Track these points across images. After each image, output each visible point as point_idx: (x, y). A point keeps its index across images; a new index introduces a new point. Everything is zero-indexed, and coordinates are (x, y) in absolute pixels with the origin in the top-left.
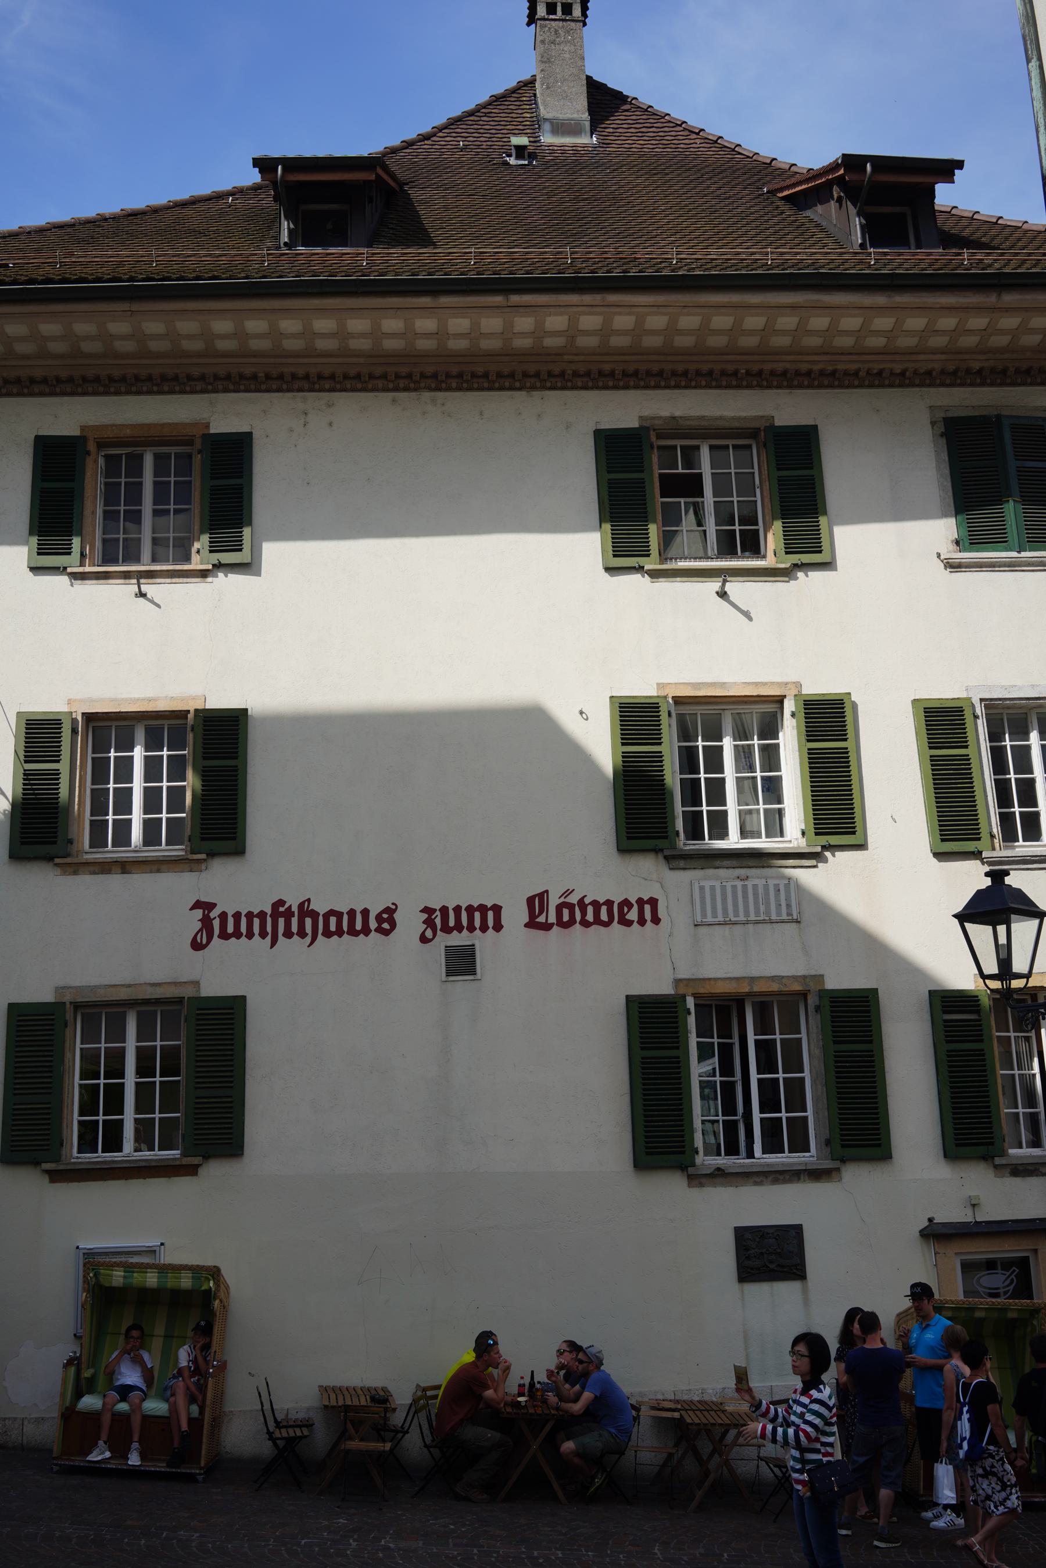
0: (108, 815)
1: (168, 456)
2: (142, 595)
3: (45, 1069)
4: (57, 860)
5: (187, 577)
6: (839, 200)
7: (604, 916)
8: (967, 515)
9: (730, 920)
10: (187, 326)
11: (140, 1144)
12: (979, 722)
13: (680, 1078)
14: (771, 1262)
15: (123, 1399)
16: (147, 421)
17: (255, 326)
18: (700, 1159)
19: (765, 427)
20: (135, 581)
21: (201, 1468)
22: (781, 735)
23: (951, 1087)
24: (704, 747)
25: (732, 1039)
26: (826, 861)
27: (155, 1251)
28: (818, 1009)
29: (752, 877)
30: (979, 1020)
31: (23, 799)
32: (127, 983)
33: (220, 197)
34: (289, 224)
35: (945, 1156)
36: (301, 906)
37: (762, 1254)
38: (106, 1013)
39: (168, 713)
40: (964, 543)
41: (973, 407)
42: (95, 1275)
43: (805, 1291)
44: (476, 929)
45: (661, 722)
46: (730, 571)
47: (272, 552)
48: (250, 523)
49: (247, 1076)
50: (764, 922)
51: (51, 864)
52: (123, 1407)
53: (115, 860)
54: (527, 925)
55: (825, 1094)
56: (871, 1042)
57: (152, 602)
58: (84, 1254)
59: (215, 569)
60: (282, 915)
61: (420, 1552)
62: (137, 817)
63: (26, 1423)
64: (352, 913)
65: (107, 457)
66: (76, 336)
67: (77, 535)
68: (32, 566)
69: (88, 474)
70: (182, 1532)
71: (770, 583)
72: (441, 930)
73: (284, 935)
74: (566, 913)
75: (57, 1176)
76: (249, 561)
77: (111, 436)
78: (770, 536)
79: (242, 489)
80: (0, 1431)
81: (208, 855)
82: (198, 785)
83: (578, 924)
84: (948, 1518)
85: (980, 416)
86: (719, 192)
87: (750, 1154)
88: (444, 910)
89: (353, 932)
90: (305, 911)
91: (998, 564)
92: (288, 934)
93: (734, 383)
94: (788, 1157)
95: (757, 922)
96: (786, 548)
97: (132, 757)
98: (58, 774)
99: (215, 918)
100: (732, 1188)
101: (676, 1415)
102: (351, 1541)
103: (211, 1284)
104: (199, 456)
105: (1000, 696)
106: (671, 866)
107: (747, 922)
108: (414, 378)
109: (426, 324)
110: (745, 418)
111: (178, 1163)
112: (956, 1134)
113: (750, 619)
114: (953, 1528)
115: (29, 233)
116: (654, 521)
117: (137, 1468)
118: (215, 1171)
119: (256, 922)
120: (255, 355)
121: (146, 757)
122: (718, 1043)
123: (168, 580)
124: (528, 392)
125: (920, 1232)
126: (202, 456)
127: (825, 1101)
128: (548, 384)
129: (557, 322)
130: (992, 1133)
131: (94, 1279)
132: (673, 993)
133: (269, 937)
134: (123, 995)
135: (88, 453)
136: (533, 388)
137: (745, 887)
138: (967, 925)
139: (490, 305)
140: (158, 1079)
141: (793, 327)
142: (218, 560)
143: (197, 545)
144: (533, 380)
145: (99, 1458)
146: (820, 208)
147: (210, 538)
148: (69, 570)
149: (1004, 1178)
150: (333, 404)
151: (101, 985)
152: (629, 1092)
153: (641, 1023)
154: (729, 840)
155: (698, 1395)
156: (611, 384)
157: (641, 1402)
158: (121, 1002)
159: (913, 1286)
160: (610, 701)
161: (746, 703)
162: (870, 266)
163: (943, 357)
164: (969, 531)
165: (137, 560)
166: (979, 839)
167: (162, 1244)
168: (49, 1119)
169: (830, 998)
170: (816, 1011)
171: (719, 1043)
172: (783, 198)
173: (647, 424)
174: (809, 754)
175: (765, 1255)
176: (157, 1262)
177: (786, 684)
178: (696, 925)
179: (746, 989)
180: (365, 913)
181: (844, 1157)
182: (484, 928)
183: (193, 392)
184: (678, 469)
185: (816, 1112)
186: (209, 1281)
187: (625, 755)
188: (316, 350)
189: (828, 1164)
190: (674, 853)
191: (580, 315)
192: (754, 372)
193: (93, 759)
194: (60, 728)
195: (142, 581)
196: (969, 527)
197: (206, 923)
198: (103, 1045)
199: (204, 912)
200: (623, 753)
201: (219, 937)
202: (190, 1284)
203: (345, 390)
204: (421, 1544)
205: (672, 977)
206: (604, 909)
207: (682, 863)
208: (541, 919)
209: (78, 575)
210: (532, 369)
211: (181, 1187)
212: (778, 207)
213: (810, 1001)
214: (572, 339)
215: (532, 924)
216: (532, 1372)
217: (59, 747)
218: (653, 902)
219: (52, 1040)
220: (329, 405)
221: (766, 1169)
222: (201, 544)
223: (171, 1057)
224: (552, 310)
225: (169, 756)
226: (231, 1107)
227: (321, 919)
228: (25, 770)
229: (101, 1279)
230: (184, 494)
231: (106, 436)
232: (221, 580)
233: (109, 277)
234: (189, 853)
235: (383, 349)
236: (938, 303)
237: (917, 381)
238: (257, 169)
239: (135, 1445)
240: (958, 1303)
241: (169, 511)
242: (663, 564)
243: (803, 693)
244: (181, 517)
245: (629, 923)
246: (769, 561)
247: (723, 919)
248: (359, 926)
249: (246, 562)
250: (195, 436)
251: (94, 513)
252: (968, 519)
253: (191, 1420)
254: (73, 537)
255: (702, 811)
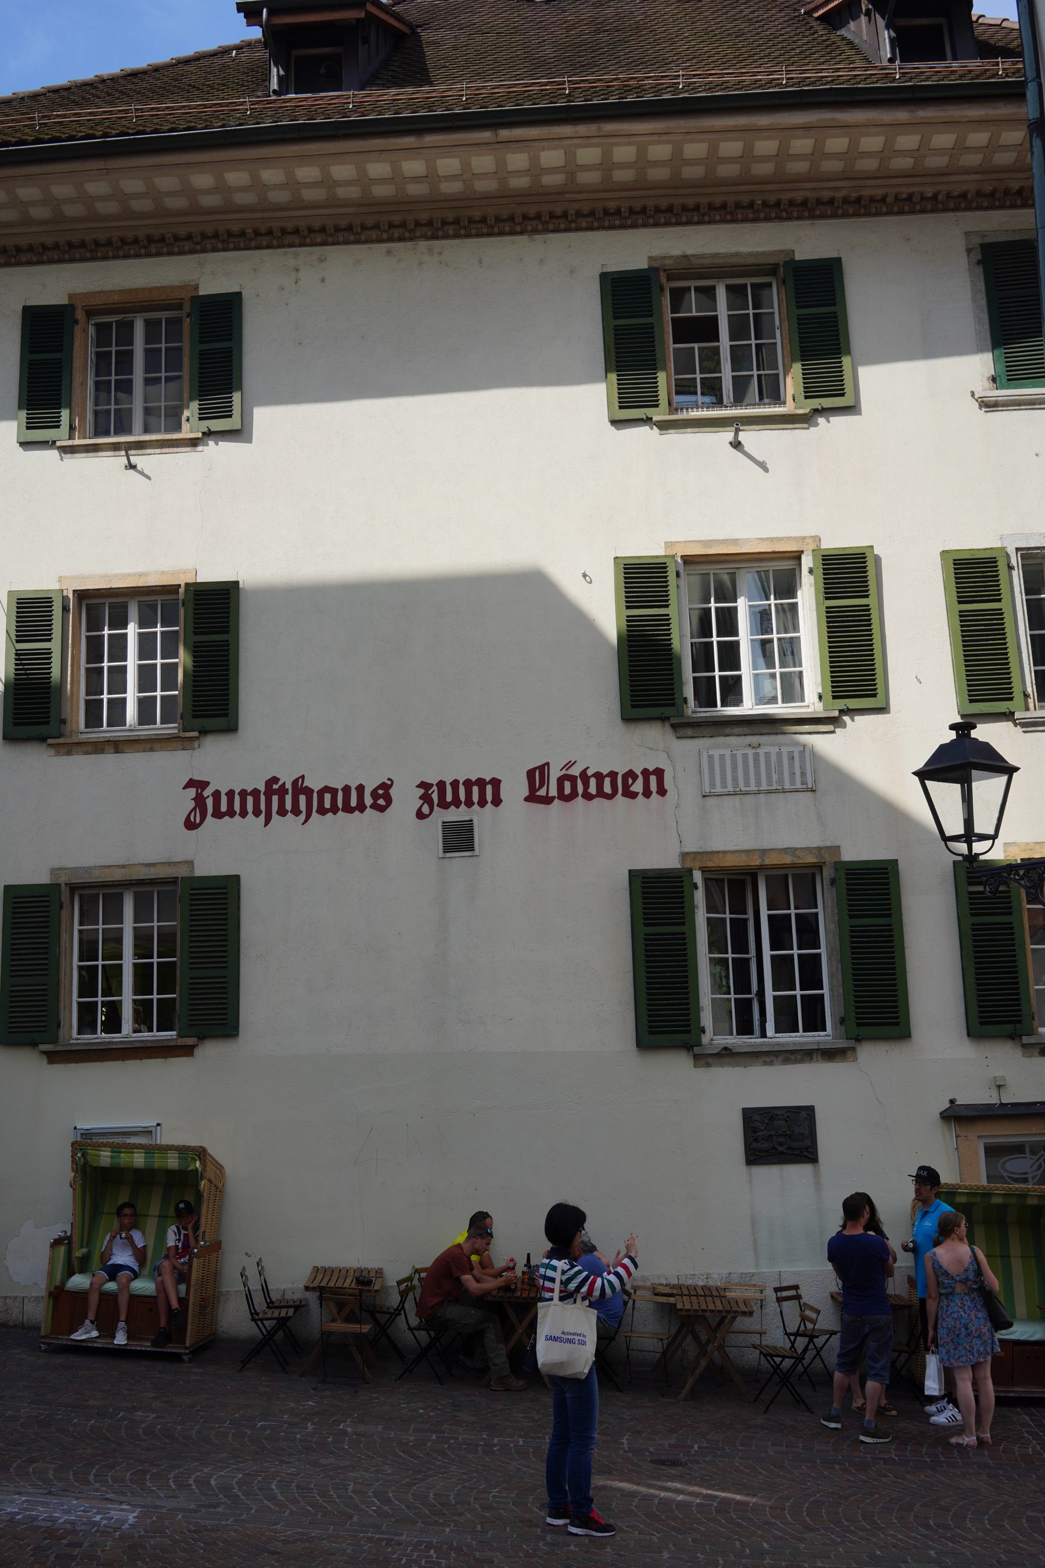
0: (102, 694)
1: (159, 321)
2: (132, 467)
3: (41, 951)
4: (50, 741)
5: (177, 446)
6: (868, 13)
7: (607, 789)
8: (1005, 349)
9: (741, 791)
10: (166, 182)
11: (140, 1025)
12: (1015, 573)
13: (685, 955)
14: (781, 1144)
15: (112, 1278)
16: (135, 286)
17: (236, 178)
18: (705, 1039)
19: (785, 262)
20: (123, 453)
21: (186, 1348)
22: (799, 593)
23: (976, 963)
24: (717, 609)
25: (746, 914)
26: (844, 725)
27: (151, 1131)
28: (833, 882)
29: (765, 745)
30: (1009, 892)
31: (16, 679)
32: (121, 863)
33: (225, 52)
34: (278, 71)
35: (969, 1035)
36: (295, 783)
37: (771, 1136)
38: (103, 894)
39: (159, 588)
40: (1001, 379)
41: (1014, 231)
42: (83, 1155)
43: (817, 1175)
44: (474, 804)
45: (669, 583)
46: (745, 420)
47: (263, 417)
48: (240, 388)
49: (242, 956)
50: (776, 791)
51: (45, 745)
52: (111, 1286)
53: (107, 739)
54: (527, 799)
55: (840, 971)
56: (889, 916)
57: (142, 473)
58: (82, 1134)
59: (206, 438)
60: (276, 792)
61: (375, 1437)
62: (131, 695)
63: (26, 1301)
64: (347, 789)
65: (98, 326)
66: (56, 199)
67: (65, 407)
68: (22, 441)
69: (77, 344)
70: (139, 1413)
71: (789, 431)
72: (438, 806)
73: (278, 813)
74: (567, 785)
75: (54, 1057)
76: (239, 427)
77: (99, 303)
78: (789, 380)
79: (231, 352)
80: (2, 1309)
81: (200, 732)
82: (190, 663)
83: (580, 797)
84: (950, 1414)
85: (1021, 241)
86: (751, 16)
87: (763, 1034)
88: (441, 785)
89: (348, 809)
90: (299, 788)
91: (1038, 401)
92: (282, 812)
93: (751, 216)
94: (802, 1036)
95: (769, 792)
96: (805, 392)
97: (126, 634)
98: (50, 653)
99: (209, 796)
100: (740, 1068)
101: (672, 1300)
102: (309, 1424)
103: (198, 1164)
104: (188, 319)
105: (1038, 545)
106: (678, 735)
107: (759, 792)
108: (408, 226)
109: (414, 167)
110: (763, 254)
111: (173, 1043)
112: (980, 1012)
113: (766, 470)
114: (955, 1423)
115: (23, 99)
116: (664, 368)
117: (123, 1347)
118: (210, 1051)
119: (250, 800)
120: (243, 209)
121: (140, 634)
122: (730, 919)
123: (158, 451)
124: (529, 236)
125: (941, 1114)
126: (191, 320)
127: (840, 978)
128: (551, 227)
129: (552, 157)
130: (1020, 1010)
131: (82, 1160)
132: (679, 867)
133: (263, 816)
134: (117, 875)
135: (76, 322)
136: (535, 231)
137: (756, 756)
138: (929, 784)
139: (479, 142)
140: (155, 960)
141: (809, 150)
142: (208, 427)
143: (186, 413)
144: (535, 223)
145: (84, 1337)
146: (852, 25)
147: (200, 405)
148: (58, 444)
149: (1033, 1058)
150: (325, 259)
151: (95, 867)
152: (632, 969)
153: (644, 898)
154: (743, 706)
155: (702, 1280)
156: (617, 223)
157: (636, 1286)
158: (116, 883)
159: (921, 1168)
160: (615, 562)
161: (761, 560)
162: (894, 80)
163: (978, 177)
164: (1007, 367)
165: (129, 431)
166: (1011, 699)
167: (158, 1125)
168: (46, 1000)
169: (846, 870)
170: (832, 884)
171: (731, 919)
172: (818, 19)
173: (656, 265)
174: (827, 612)
175: (774, 1138)
176: (154, 1143)
177: (804, 538)
178: (704, 796)
179: (756, 862)
180: (360, 789)
181: (859, 1036)
182: (482, 803)
183: (181, 253)
184: (691, 312)
185: (831, 990)
186: (196, 1160)
187: (630, 619)
188: (304, 201)
189: (842, 1043)
190: (682, 721)
191: (576, 148)
192: (772, 203)
193: (87, 637)
194: (51, 607)
195: (131, 452)
196: (1007, 362)
197: (200, 801)
198: (101, 927)
199: (197, 791)
200: (627, 616)
201: (213, 815)
202: (177, 1164)
203: (337, 243)
204: (380, 1428)
205: (678, 851)
206: (607, 781)
207: (689, 732)
208: (542, 792)
209: (67, 448)
210: (532, 210)
211: (178, 1065)
212: (812, 27)
213: (825, 874)
214: (571, 175)
215: (532, 798)
216: (529, 1255)
217: (50, 625)
218: (659, 773)
219: (48, 922)
220: (322, 260)
221: (776, 1049)
222: (191, 411)
223: (167, 941)
224: (545, 144)
225: (162, 633)
226: (225, 988)
227: (315, 796)
228: (16, 650)
229: (89, 1160)
230: (174, 360)
231: (94, 303)
232: (213, 449)
233: (82, 134)
234: (181, 731)
235: (373, 197)
236: (966, 116)
237: (951, 205)
238: (242, 14)
239: (122, 1325)
240: (972, 1188)
241: (160, 378)
242: (673, 414)
243: (822, 548)
244: (173, 385)
245: (633, 795)
246: (789, 408)
247: (732, 790)
248: (354, 803)
249: (236, 428)
250: (184, 299)
251: (84, 384)
252: (1005, 353)
253: (180, 1300)
254: (62, 410)
255: (714, 677)
